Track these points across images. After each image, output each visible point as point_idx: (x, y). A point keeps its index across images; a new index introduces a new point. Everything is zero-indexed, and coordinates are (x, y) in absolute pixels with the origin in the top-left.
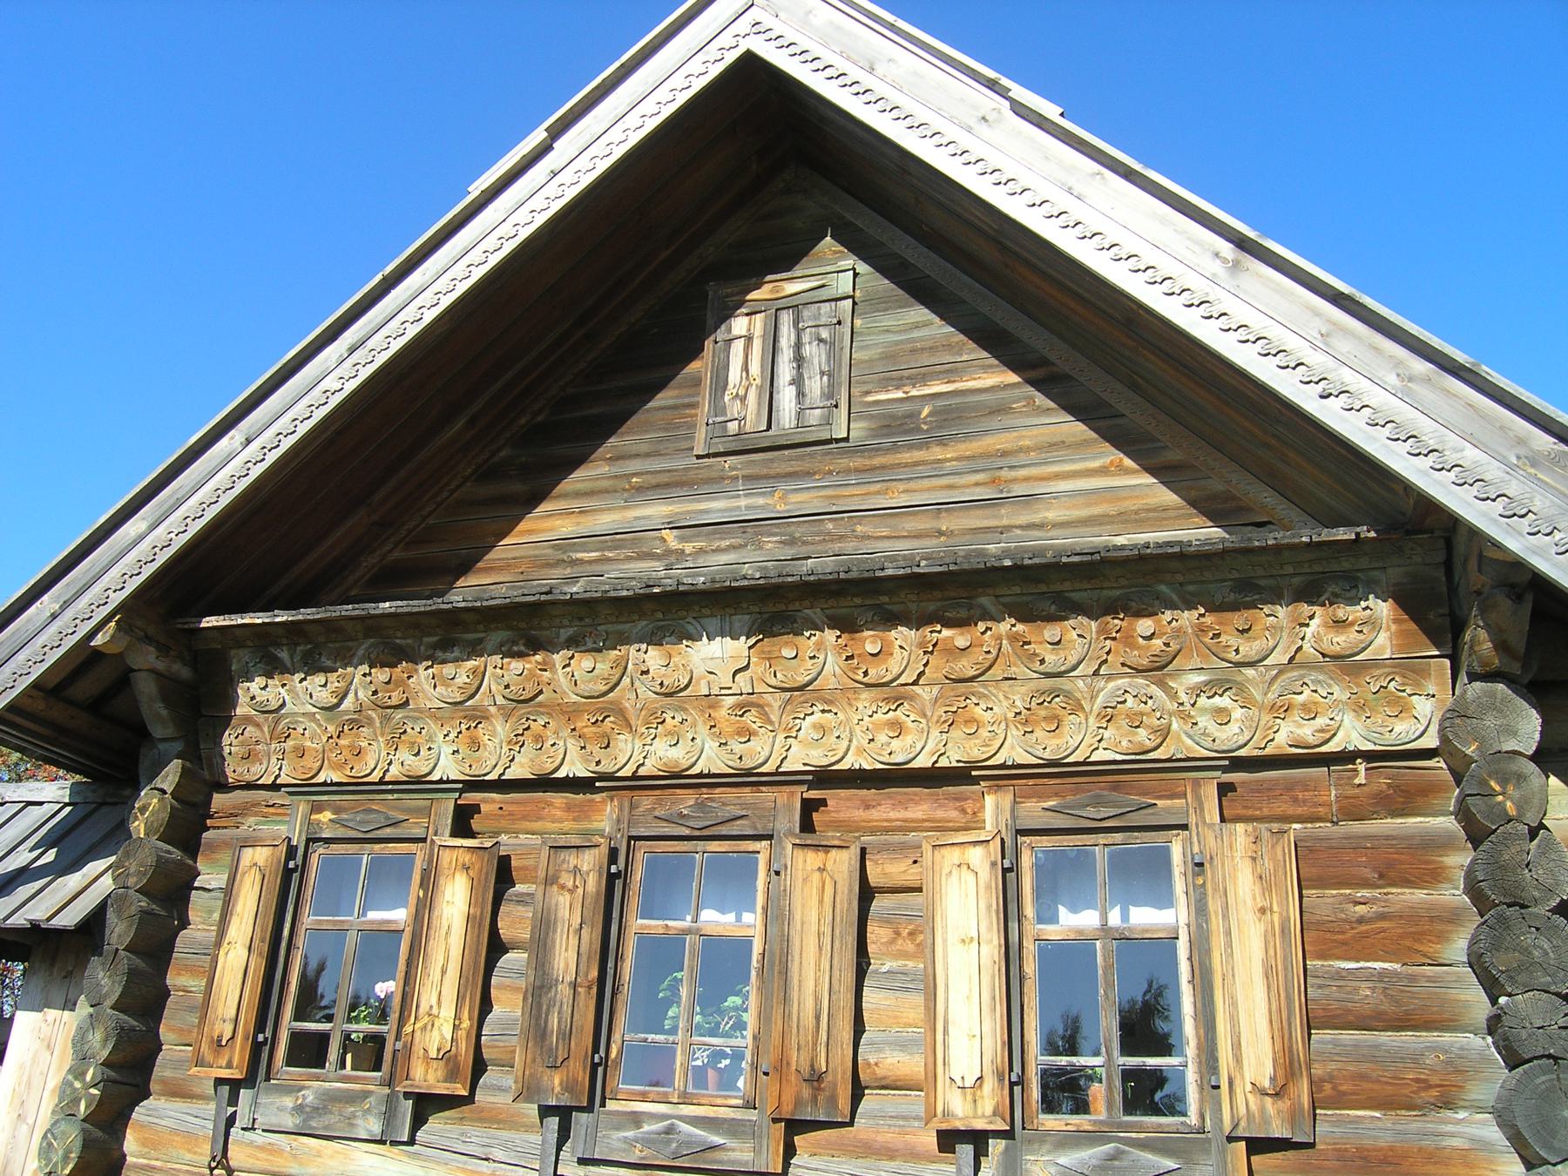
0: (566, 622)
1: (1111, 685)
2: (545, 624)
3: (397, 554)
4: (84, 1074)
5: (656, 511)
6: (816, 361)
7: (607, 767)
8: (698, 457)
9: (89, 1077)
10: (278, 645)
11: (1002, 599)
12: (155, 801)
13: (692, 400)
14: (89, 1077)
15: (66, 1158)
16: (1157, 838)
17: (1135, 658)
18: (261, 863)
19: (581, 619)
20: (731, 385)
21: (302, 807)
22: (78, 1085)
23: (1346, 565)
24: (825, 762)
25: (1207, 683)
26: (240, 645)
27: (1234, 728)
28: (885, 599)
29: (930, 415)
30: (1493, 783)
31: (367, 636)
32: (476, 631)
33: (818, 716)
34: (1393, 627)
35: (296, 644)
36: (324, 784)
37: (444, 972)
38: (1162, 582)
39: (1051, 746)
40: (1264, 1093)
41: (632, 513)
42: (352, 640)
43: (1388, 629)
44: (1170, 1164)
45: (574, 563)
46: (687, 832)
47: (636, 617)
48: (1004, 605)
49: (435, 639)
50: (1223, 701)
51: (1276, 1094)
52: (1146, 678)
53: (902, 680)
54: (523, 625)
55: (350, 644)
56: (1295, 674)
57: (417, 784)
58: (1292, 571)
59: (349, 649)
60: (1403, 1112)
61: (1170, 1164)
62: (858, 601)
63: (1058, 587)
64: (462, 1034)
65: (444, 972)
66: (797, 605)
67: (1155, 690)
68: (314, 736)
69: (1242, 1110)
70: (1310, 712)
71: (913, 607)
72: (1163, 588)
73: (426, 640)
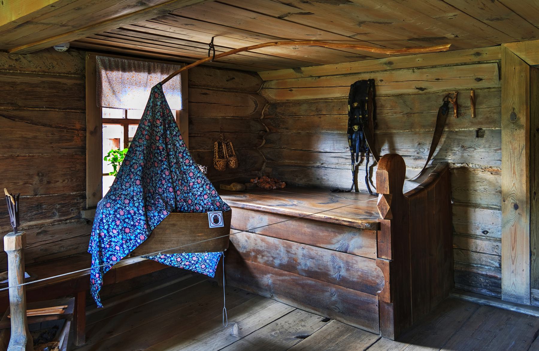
44: (268, 130)
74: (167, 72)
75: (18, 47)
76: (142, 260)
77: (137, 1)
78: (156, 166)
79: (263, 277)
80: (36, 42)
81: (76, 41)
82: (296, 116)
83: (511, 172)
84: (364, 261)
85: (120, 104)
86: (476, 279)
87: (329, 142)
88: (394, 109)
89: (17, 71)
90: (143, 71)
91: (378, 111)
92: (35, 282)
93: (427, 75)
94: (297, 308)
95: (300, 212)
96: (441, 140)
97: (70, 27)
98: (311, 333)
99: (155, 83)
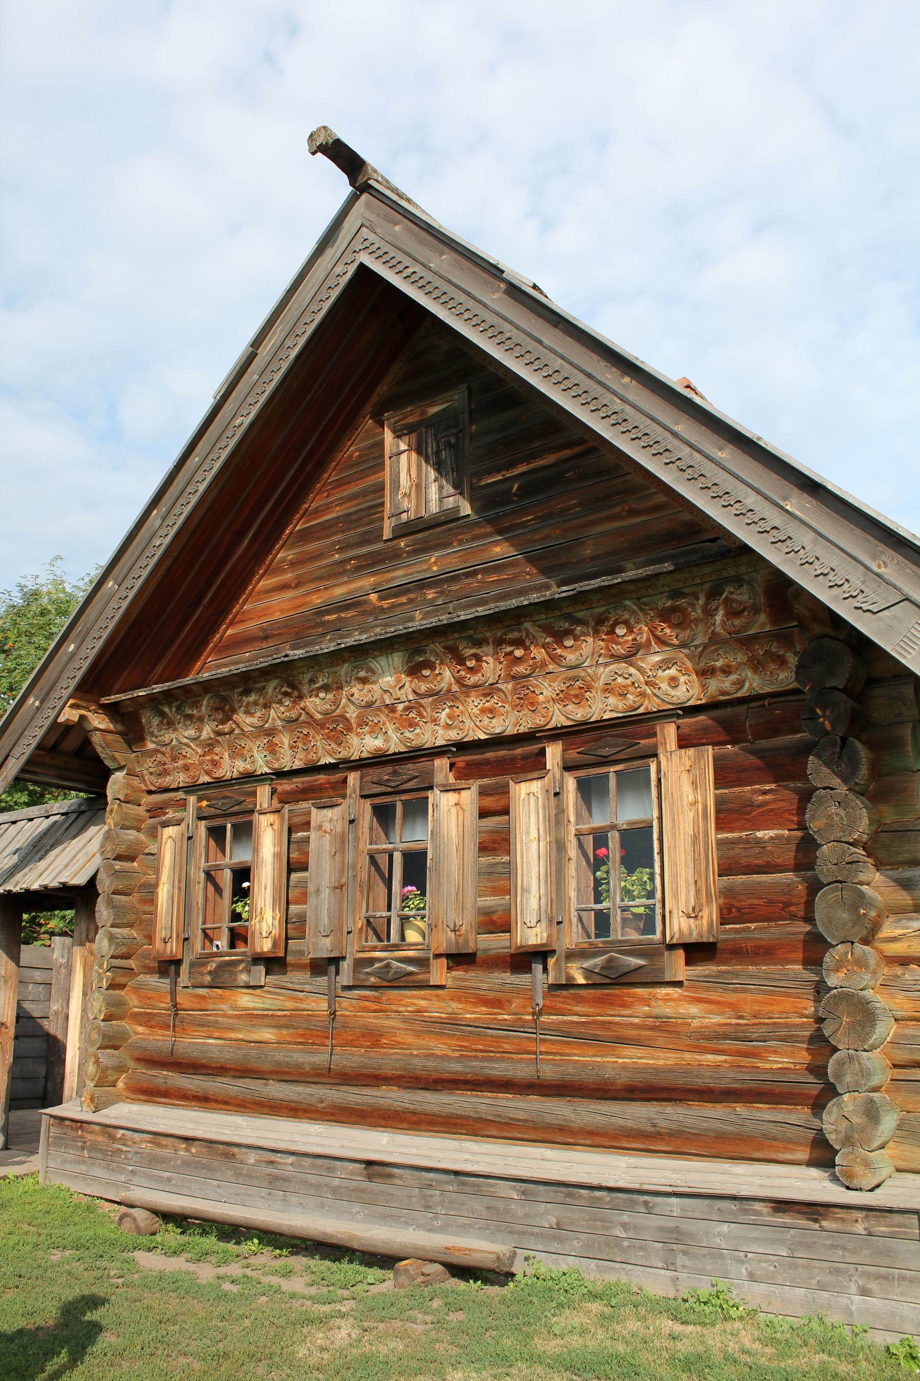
0: (305, 670)
1: (607, 669)
2: (295, 673)
3: (229, 632)
4: (103, 964)
5: (366, 582)
6: (449, 462)
7: (344, 754)
8: (386, 541)
9: (105, 967)
10: (163, 704)
11: (537, 623)
12: (116, 806)
13: (378, 501)
14: (105, 967)
15: (100, 1011)
16: (423, 764)
17: (619, 650)
18: (174, 836)
19: (313, 667)
20: (401, 487)
21: (192, 799)
22: (101, 971)
23: (732, 573)
24: (459, 737)
25: (662, 661)
26: (142, 706)
27: (683, 688)
28: (471, 632)
29: (517, 490)
30: (818, 710)
31: (206, 693)
32: (260, 682)
33: (447, 710)
34: (768, 609)
35: (172, 703)
36: (203, 784)
37: (265, 888)
38: (626, 599)
39: (578, 714)
40: (689, 917)
41: (352, 586)
42: (197, 696)
43: (766, 612)
44: (642, 962)
45: (323, 624)
46: (390, 789)
47: (340, 662)
48: (539, 626)
49: (240, 690)
50: (673, 672)
51: (696, 917)
52: (626, 662)
53: (585, 665)
54: (284, 675)
55: (198, 698)
56: (714, 648)
57: (249, 778)
58: (700, 581)
59: (198, 702)
60: (781, 923)
61: (642, 962)
62: (457, 635)
63: (566, 611)
64: (277, 922)
65: (265, 888)
66: (424, 643)
67: (632, 670)
68: (194, 754)
69: (676, 928)
70: (727, 671)
71: (488, 634)
72: (627, 603)
73: (236, 691)
74: (517, 551)
75: (636, 577)
76: (50, 1109)
77: (3, 987)
78: (327, 835)
79: (111, 968)
80: (439, 239)
81: (570, 898)
82: (529, 1229)
83: (296, 608)
84: (223, 982)
85: (307, 1325)
86: (660, 605)
87: (51, 1322)
88: (148, 1077)
89: (769, 704)
90: (479, 503)
91: (90, 589)
92: (309, 447)
93: (287, 659)
94: (907, 599)
95: (221, 1211)
96: (667, 1106)
97: (57, 818)
98: (886, 1034)
99: (385, 1141)
